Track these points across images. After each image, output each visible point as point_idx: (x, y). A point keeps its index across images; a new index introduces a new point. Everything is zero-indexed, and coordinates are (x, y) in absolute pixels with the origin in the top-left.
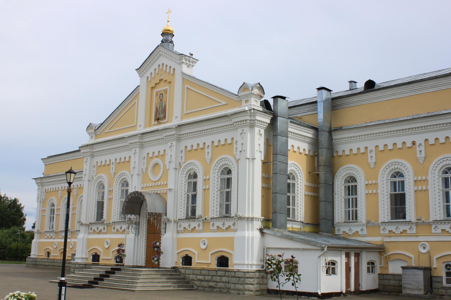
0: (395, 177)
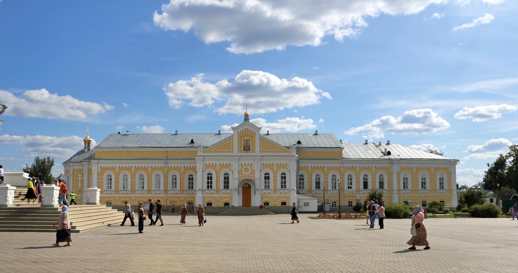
0: (365, 176)
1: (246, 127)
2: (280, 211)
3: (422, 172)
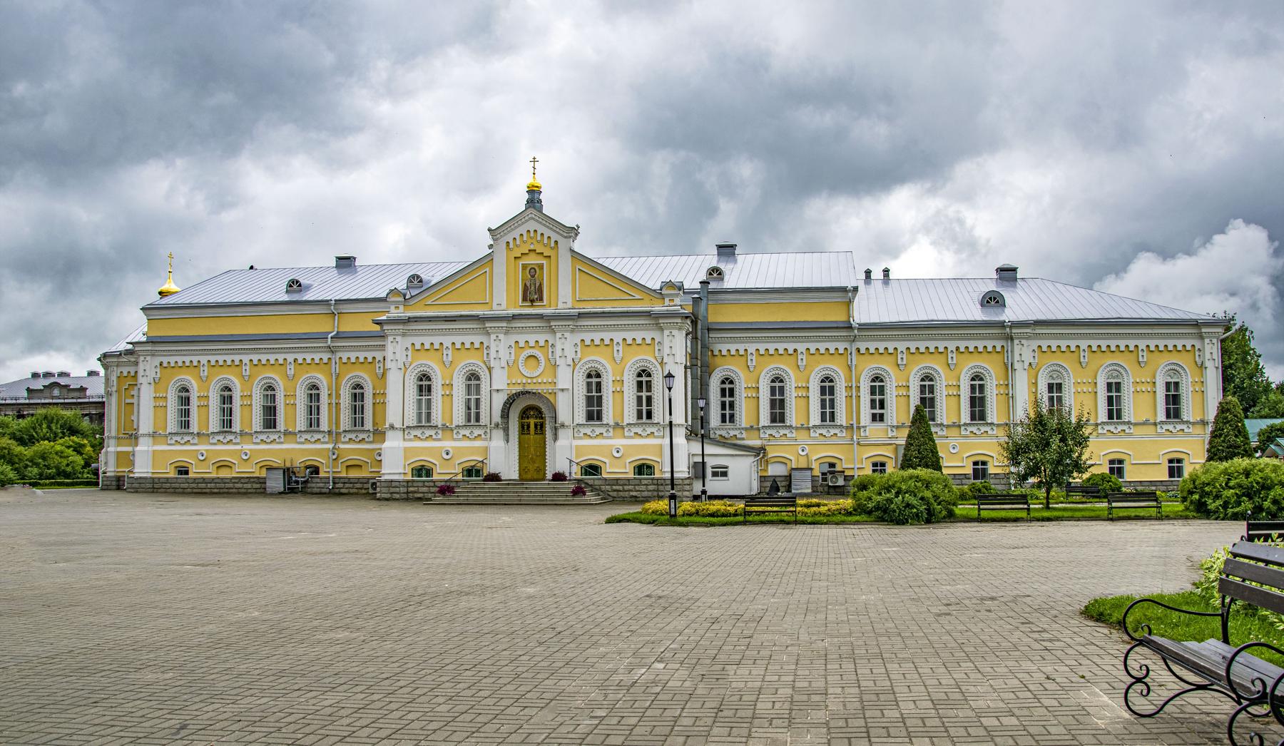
0: (311, 390)
1: (532, 226)
2: (632, 493)
3: (215, 381)
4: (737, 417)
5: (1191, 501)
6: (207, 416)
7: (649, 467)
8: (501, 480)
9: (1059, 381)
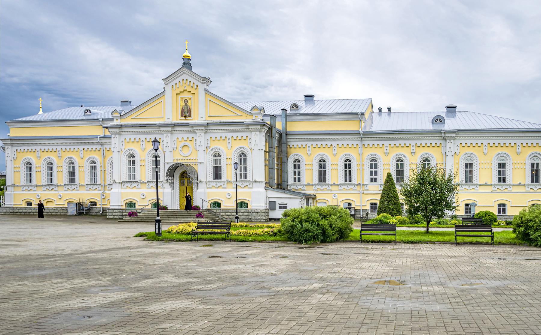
4: (301, 180)
5: (519, 232)
6: (39, 177)
7: (245, 204)
8: (168, 210)
9: (471, 162)
